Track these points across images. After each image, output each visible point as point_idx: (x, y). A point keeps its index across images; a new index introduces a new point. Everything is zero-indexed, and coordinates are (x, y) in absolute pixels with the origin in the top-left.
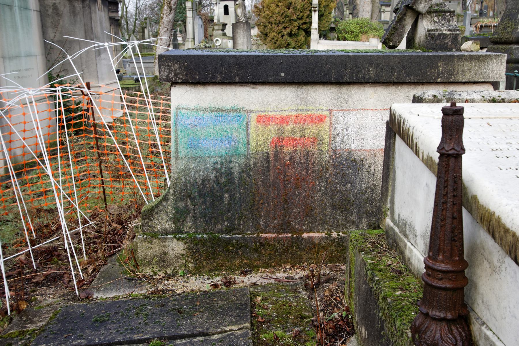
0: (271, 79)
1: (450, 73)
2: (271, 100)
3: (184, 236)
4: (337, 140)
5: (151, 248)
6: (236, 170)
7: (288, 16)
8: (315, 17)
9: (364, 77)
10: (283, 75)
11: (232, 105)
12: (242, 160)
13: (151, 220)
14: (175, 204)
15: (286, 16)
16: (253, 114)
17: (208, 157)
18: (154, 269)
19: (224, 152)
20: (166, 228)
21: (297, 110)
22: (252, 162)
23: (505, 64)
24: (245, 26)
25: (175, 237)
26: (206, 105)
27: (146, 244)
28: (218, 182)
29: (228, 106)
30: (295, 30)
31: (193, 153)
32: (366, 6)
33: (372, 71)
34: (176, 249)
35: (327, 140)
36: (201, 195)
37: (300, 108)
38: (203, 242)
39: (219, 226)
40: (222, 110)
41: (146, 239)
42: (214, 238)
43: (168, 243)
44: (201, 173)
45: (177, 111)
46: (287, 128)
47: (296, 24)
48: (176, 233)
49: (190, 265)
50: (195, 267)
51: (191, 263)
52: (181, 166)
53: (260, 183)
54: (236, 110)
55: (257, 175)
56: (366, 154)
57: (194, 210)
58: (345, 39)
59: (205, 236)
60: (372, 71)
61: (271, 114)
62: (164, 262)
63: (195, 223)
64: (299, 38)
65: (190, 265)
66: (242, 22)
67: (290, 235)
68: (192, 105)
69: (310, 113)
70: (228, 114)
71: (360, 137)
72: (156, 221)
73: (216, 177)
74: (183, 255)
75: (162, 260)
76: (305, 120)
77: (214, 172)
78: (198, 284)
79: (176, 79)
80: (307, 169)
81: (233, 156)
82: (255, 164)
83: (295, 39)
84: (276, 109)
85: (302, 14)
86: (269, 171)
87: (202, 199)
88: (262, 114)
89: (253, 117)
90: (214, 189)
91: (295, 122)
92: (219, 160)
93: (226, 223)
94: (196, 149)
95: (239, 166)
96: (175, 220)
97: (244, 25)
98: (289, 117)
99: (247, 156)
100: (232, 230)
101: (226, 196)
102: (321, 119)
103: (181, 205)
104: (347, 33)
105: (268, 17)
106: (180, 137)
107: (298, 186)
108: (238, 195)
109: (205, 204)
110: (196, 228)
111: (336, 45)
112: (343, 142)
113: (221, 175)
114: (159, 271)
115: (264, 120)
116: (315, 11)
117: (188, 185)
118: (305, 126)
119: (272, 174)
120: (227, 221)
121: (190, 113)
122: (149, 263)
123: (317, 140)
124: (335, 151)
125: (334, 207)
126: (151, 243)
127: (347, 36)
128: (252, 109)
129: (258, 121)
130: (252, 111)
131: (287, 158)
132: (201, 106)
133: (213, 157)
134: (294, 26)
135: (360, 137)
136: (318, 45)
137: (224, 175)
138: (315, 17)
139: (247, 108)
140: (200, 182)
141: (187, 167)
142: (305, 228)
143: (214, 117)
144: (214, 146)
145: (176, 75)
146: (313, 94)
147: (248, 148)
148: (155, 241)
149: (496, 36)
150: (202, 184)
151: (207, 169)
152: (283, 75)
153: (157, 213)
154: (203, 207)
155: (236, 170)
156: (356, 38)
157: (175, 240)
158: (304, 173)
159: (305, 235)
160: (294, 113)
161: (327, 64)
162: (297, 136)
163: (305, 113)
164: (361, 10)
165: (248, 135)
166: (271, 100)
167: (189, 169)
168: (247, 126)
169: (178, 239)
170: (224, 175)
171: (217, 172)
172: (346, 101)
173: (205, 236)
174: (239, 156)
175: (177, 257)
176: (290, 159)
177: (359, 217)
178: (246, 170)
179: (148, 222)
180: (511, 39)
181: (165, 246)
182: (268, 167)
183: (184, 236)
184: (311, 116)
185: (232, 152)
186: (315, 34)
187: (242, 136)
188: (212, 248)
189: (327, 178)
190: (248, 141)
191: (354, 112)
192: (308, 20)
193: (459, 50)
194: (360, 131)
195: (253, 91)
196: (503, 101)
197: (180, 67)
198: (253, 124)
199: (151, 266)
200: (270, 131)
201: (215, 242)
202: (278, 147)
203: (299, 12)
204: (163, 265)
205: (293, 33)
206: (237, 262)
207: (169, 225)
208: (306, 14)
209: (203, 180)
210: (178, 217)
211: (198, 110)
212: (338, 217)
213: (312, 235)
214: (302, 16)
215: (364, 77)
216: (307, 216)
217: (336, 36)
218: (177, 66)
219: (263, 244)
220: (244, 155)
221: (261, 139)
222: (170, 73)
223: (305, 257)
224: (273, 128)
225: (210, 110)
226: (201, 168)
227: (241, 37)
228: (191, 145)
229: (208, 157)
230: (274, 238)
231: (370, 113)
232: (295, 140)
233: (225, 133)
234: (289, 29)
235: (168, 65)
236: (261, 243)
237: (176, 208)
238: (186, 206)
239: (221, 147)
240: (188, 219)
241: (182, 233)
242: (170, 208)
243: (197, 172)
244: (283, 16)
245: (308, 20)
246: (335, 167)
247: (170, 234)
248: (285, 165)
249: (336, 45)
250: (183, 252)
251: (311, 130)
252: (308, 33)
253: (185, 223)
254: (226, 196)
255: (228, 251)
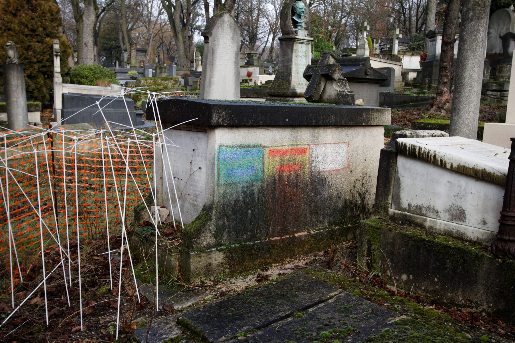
0: (281, 123)
1: (368, 119)
2: (277, 138)
3: (223, 247)
4: (313, 165)
5: (200, 262)
6: (256, 191)
7: (27, 59)
8: (57, 62)
9: (329, 122)
10: (287, 120)
11: (254, 142)
12: (260, 184)
13: (199, 238)
14: (217, 222)
15: (26, 58)
16: (266, 149)
17: (239, 183)
18: (202, 279)
19: (249, 178)
20: (209, 243)
21: (291, 145)
22: (265, 185)
23: (390, 114)
24: (19, 68)
25: (217, 250)
26: (238, 143)
27: (197, 259)
28: (244, 202)
29: (252, 144)
30: (35, 72)
31: (229, 181)
32: (89, 54)
33: (333, 118)
34: (218, 259)
35: (308, 165)
36: (234, 213)
37: (293, 143)
38: (236, 250)
39: (245, 237)
40: (248, 146)
41: (197, 254)
42: (243, 246)
43: (213, 255)
44: (234, 196)
45: (220, 148)
46: (286, 158)
47: (36, 66)
48: (217, 245)
49: (227, 270)
50: (230, 272)
51: (228, 269)
52: (221, 192)
53: (270, 200)
54: (256, 146)
55: (269, 194)
56: (327, 174)
57: (229, 226)
58: (80, 83)
59: (237, 245)
60: (333, 118)
61: (277, 148)
62: (209, 271)
63: (230, 236)
64: (39, 80)
65: (227, 270)
66: (15, 63)
67: (288, 236)
68: (229, 143)
69: (298, 147)
70: (251, 149)
71: (324, 163)
72: (203, 238)
73: (243, 198)
74: (222, 263)
75: (208, 270)
76: (296, 152)
77: (242, 194)
78: (240, 284)
79: (223, 124)
80: (297, 187)
81: (254, 181)
82: (267, 186)
83: (34, 81)
84: (280, 145)
85: (41, 58)
86: (276, 190)
87: (234, 217)
88: (272, 148)
89: (267, 150)
90: (242, 207)
91: (291, 154)
92: (246, 185)
93: (249, 233)
94: (231, 177)
95: (258, 188)
96: (215, 236)
97: (18, 67)
98: (287, 150)
99: (263, 180)
100: (253, 238)
101: (250, 212)
102: (304, 151)
103: (220, 223)
104: (82, 77)
105: (4, 58)
106: (221, 169)
107: (291, 200)
108: (257, 211)
109: (236, 220)
110: (230, 240)
111: (81, 89)
112: (316, 166)
113: (247, 196)
114: (205, 279)
115: (273, 153)
116: (57, 56)
117: (226, 206)
118: (296, 156)
119: (277, 192)
120: (249, 231)
121: (228, 149)
122: (199, 275)
123: (302, 166)
124: (311, 172)
125: (311, 213)
126: (200, 257)
127: (82, 80)
128: (266, 145)
129: (270, 154)
130: (266, 147)
131: (286, 180)
132: (235, 144)
133: (242, 182)
134: (35, 69)
135: (324, 163)
136: (64, 88)
137: (248, 196)
138: (57, 62)
139: (263, 144)
140: (233, 203)
141: (225, 193)
142: (295, 230)
143: (243, 152)
144: (243, 174)
145: (223, 120)
146: (300, 134)
147: (263, 174)
148: (204, 255)
149: (273, 91)
150: (235, 205)
151: (238, 192)
152: (287, 120)
153: (204, 232)
154: (235, 222)
155: (256, 191)
156: (91, 83)
157: (217, 252)
158: (295, 190)
159: (296, 235)
160: (290, 147)
161: (311, 113)
162: (291, 164)
163: (296, 147)
164: (84, 56)
165: (263, 164)
166: (277, 138)
167: (226, 194)
168: (263, 158)
169: (219, 251)
170: (248, 196)
171: (244, 194)
172: (317, 138)
173: (237, 245)
174: (258, 180)
175: (219, 266)
176: (288, 181)
177: (324, 218)
178: (262, 191)
179: (197, 241)
180: (288, 94)
181: (210, 258)
182: (275, 188)
183: (223, 247)
184: (298, 149)
185: (253, 178)
186: (58, 78)
187: (260, 165)
188: (242, 254)
189: (308, 192)
190: (264, 169)
191: (321, 146)
192: (48, 64)
193: (354, 105)
194: (325, 159)
195: (267, 131)
196: (435, 136)
197: (226, 114)
198: (266, 156)
199: (199, 277)
200: (276, 161)
201: (243, 249)
202: (281, 172)
203: (39, 56)
204: (208, 275)
205: (33, 75)
206: (257, 263)
207: (212, 241)
208: (45, 58)
209: (235, 201)
210: (217, 235)
211: (233, 147)
212: (313, 219)
213: (300, 234)
214: (43, 59)
215: (329, 122)
216: (296, 221)
217: (69, 80)
218: (224, 113)
219: (273, 245)
220: (261, 180)
221: (271, 167)
222: (219, 118)
223: (297, 251)
224: (278, 158)
225: (241, 147)
226: (234, 192)
227: (15, 78)
228: (228, 175)
229: (239, 183)
230: (280, 239)
231: (329, 146)
232: (290, 166)
233: (250, 164)
234: (29, 71)
235: (218, 112)
236: (272, 245)
237: (216, 226)
238: (224, 223)
239: (247, 175)
240: (225, 234)
241: (220, 245)
242: (213, 226)
243: (232, 195)
244: (22, 58)
245: (48, 64)
246: (312, 184)
247: (214, 248)
248: (285, 185)
249: (81, 89)
250: (223, 261)
251: (299, 158)
252: (50, 76)
253: (223, 237)
254: (250, 212)
255: (252, 254)
